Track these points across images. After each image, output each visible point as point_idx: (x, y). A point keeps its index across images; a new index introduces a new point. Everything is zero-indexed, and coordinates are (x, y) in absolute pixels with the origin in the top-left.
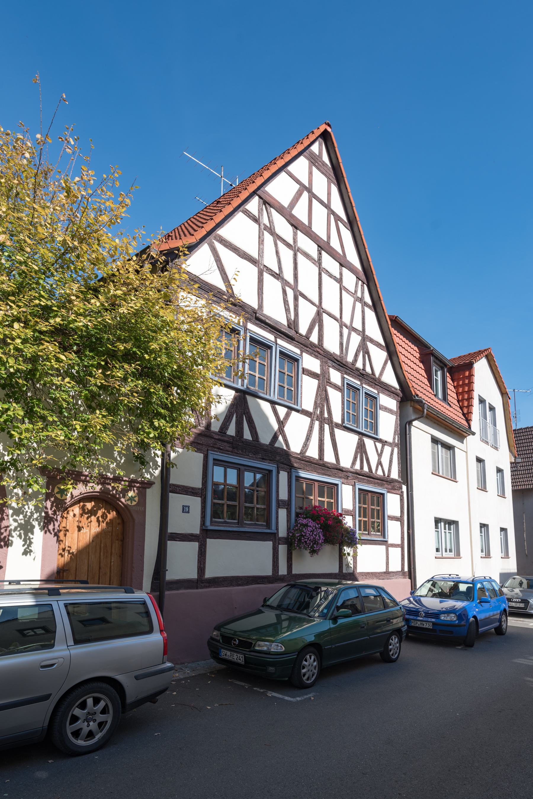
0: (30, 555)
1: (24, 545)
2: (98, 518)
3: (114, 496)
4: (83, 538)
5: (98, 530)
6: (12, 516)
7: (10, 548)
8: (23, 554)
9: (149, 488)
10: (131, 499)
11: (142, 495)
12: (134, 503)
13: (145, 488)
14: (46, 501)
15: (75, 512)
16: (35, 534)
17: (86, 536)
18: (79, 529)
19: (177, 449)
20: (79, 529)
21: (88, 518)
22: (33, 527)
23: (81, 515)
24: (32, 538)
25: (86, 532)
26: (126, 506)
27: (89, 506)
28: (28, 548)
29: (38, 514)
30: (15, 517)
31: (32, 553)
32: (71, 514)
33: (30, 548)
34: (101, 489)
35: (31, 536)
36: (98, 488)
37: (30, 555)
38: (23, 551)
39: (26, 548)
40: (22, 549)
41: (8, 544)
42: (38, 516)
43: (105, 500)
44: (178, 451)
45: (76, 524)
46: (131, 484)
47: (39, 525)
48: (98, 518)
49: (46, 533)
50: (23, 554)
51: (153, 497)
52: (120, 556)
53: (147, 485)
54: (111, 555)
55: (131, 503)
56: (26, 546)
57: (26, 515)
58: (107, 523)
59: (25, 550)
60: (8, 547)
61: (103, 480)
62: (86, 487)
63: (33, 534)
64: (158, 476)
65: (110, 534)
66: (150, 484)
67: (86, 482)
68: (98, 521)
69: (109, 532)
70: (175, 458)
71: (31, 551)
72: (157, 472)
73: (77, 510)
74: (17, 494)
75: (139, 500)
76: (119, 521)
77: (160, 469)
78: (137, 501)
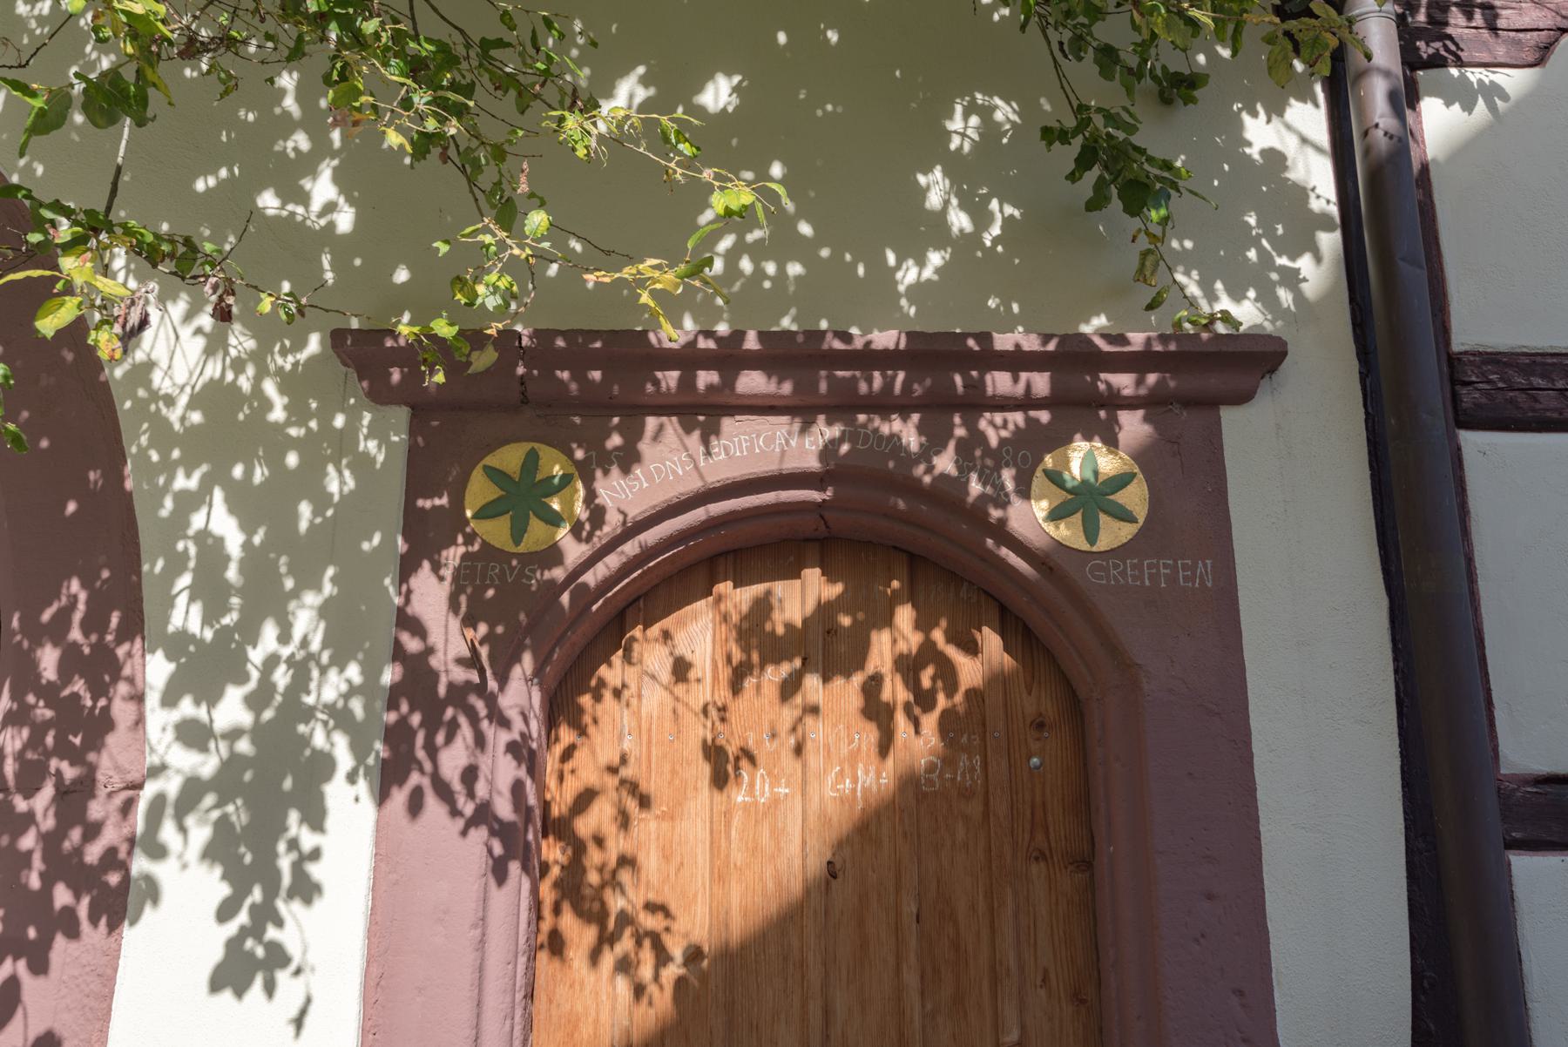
0: (270, 989)
1: (225, 913)
2: (872, 687)
3: (947, 494)
4: (754, 850)
5: (874, 779)
6: (170, 699)
7: (130, 935)
8: (217, 983)
9: (1242, 398)
10: (1087, 501)
11: (1189, 476)
12: (1113, 534)
13: (1210, 403)
14: (407, 568)
15: (682, 649)
16: (330, 823)
17: (777, 834)
18: (723, 765)
19: (1475, 75)
20: (723, 765)
21: (789, 688)
22: (324, 765)
23: (738, 677)
24: (316, 854)
25: (775, 801)
26: (1048, 560)
27: (800, 596)
28: (255, 930)
29: (354, 672)
30: (187, 707)
31: (283, 977)
32: (656, 658)
33: (272, 933)
34: (828, 451)
35: (308, 840)
36: (795, 446)
37: (270, 989)
38: (217, 954)
39: (244, 932)
40: (212, 942)
41: (117, 901)
42: (352, 691)
43: (883, 538)
44: (1492, 92)
45: (698, 731)
46: (1078, 389)
47: (359, 749)
48: (872, 687)
49: (415, 806)
50: (217, 983)
51: (1297, 483)
52: (1078, 998)
53: (1213, 375)
54: (995, 981)
55: (1091, 535)
56: (243, 918)
57: (266, 685)
58: (948, 724)
59: (233, 945)
60: (114, 926)
61: (810, 371)
62: (706, 442)
63: (316, 820)
64: (1327, 297)
65: (975, 808)
66: (1250, 362)
67: (703, 414)
68: (876, 710)
69: (966, 794)
70: (1467, 149)
71: (278, 956)
72: (1317, 270)
73: (699, 632)
74: (211, 546)
75: (1155, 502)
76: (1039, 702)
77: (1330, 241)
78: (1141, 513)
